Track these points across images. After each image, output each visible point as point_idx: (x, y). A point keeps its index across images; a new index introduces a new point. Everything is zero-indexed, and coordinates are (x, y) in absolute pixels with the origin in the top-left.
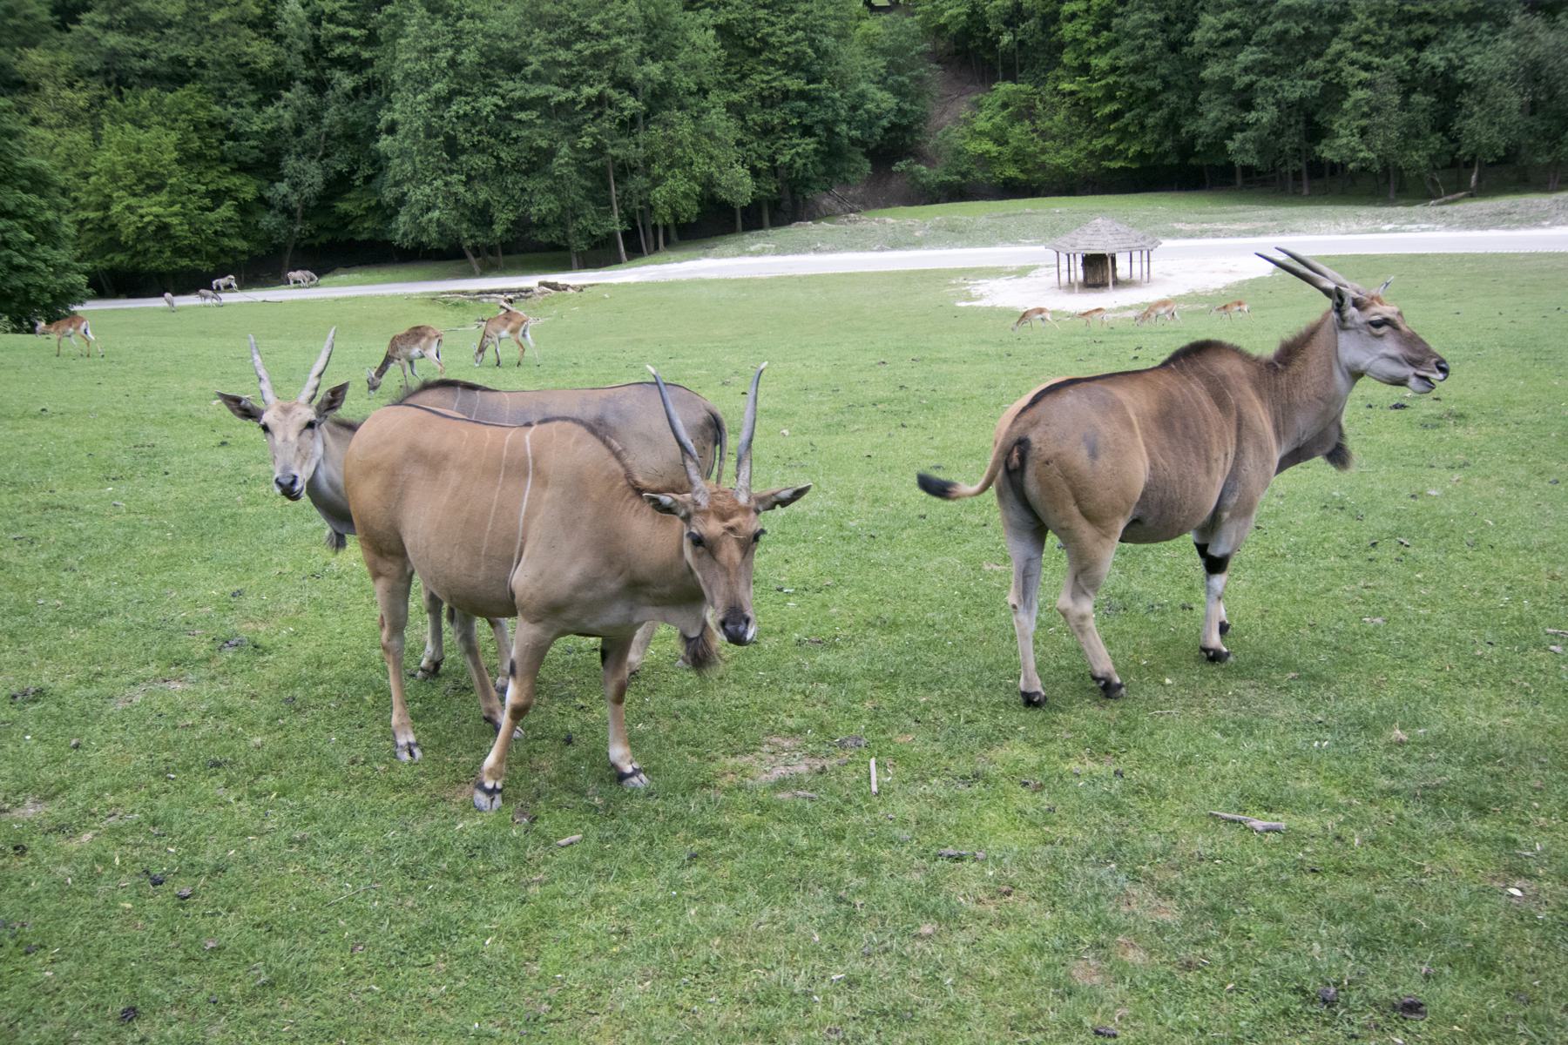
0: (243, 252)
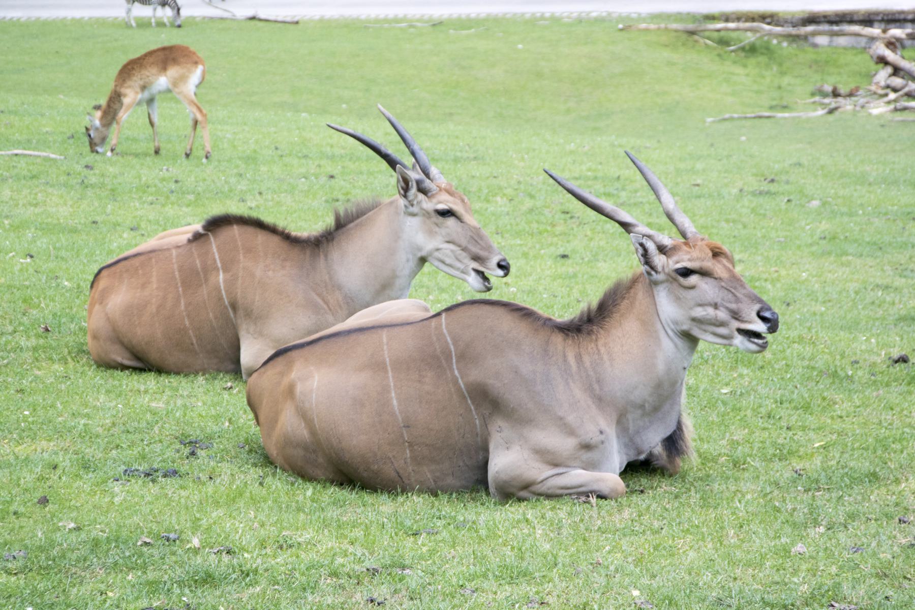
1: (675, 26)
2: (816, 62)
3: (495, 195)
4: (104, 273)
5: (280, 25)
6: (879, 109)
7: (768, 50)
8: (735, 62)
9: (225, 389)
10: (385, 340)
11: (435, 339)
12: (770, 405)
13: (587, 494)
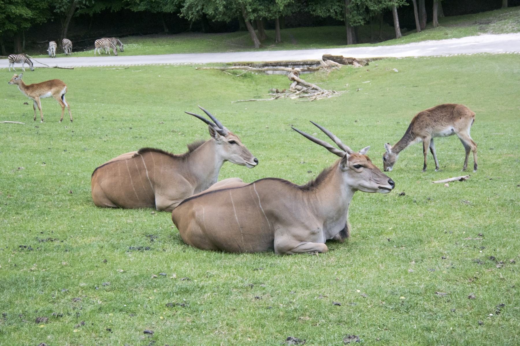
0: (26, 20)
1: (216, 68)
2: (268, 80)
3: (195, 133)
4: (99, 170)
5: (66, 70)
6: (294, 97)
7: (251, 76)
8: (239, 81)
9: (152, 214)
10: (231, 194)
11: (251, 193)
12: (364, 214)
13: (314, 252)
